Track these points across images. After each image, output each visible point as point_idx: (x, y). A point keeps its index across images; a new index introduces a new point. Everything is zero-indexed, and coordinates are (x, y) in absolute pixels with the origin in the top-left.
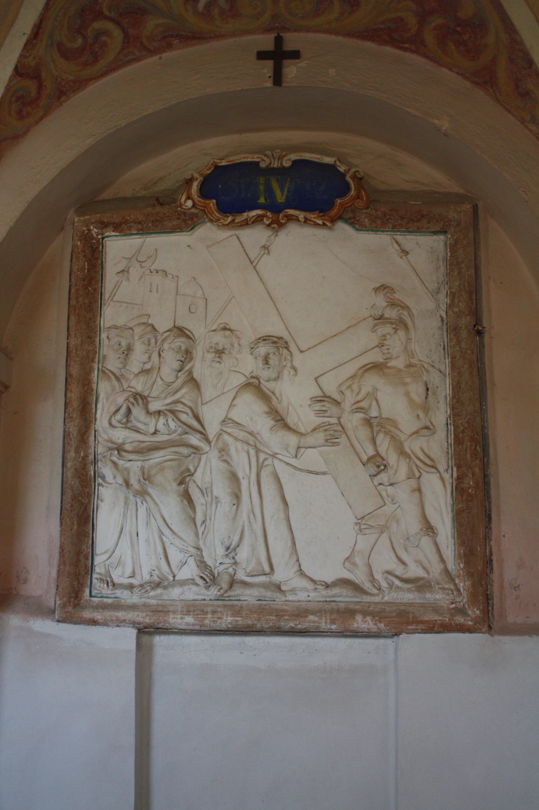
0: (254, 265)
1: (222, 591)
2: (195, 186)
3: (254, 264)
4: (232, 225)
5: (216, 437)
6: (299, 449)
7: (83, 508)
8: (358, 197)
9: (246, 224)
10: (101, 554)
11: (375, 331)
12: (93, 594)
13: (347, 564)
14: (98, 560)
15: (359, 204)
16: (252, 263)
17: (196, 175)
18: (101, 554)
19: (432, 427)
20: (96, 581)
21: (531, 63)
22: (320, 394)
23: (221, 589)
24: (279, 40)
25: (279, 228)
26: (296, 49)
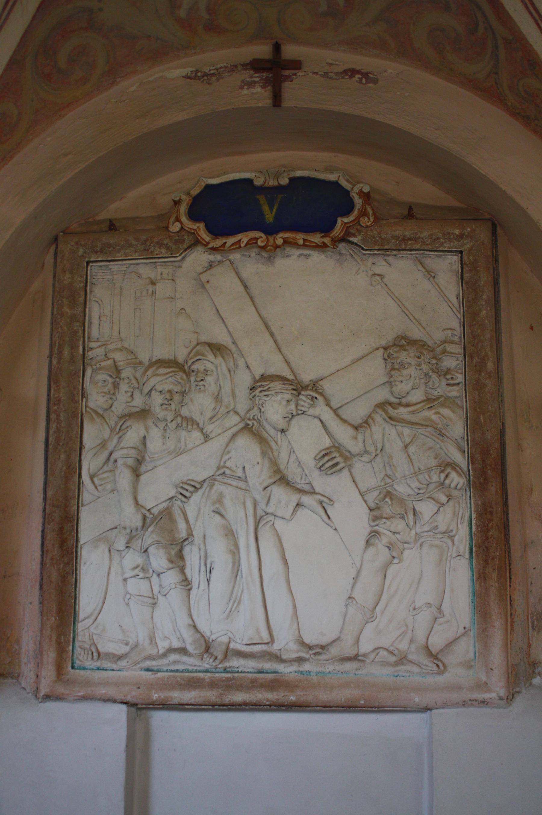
1: (217, 662)
2: (183, 208)
8: (363, 213)
10: (85, 618)
12: (76, 665)
14: (80, 626)
15: (364, 221)
17: (184, 197)
18: (85, 618)
20: (79, 649)
23: (216, 658)
24: (277, 48)
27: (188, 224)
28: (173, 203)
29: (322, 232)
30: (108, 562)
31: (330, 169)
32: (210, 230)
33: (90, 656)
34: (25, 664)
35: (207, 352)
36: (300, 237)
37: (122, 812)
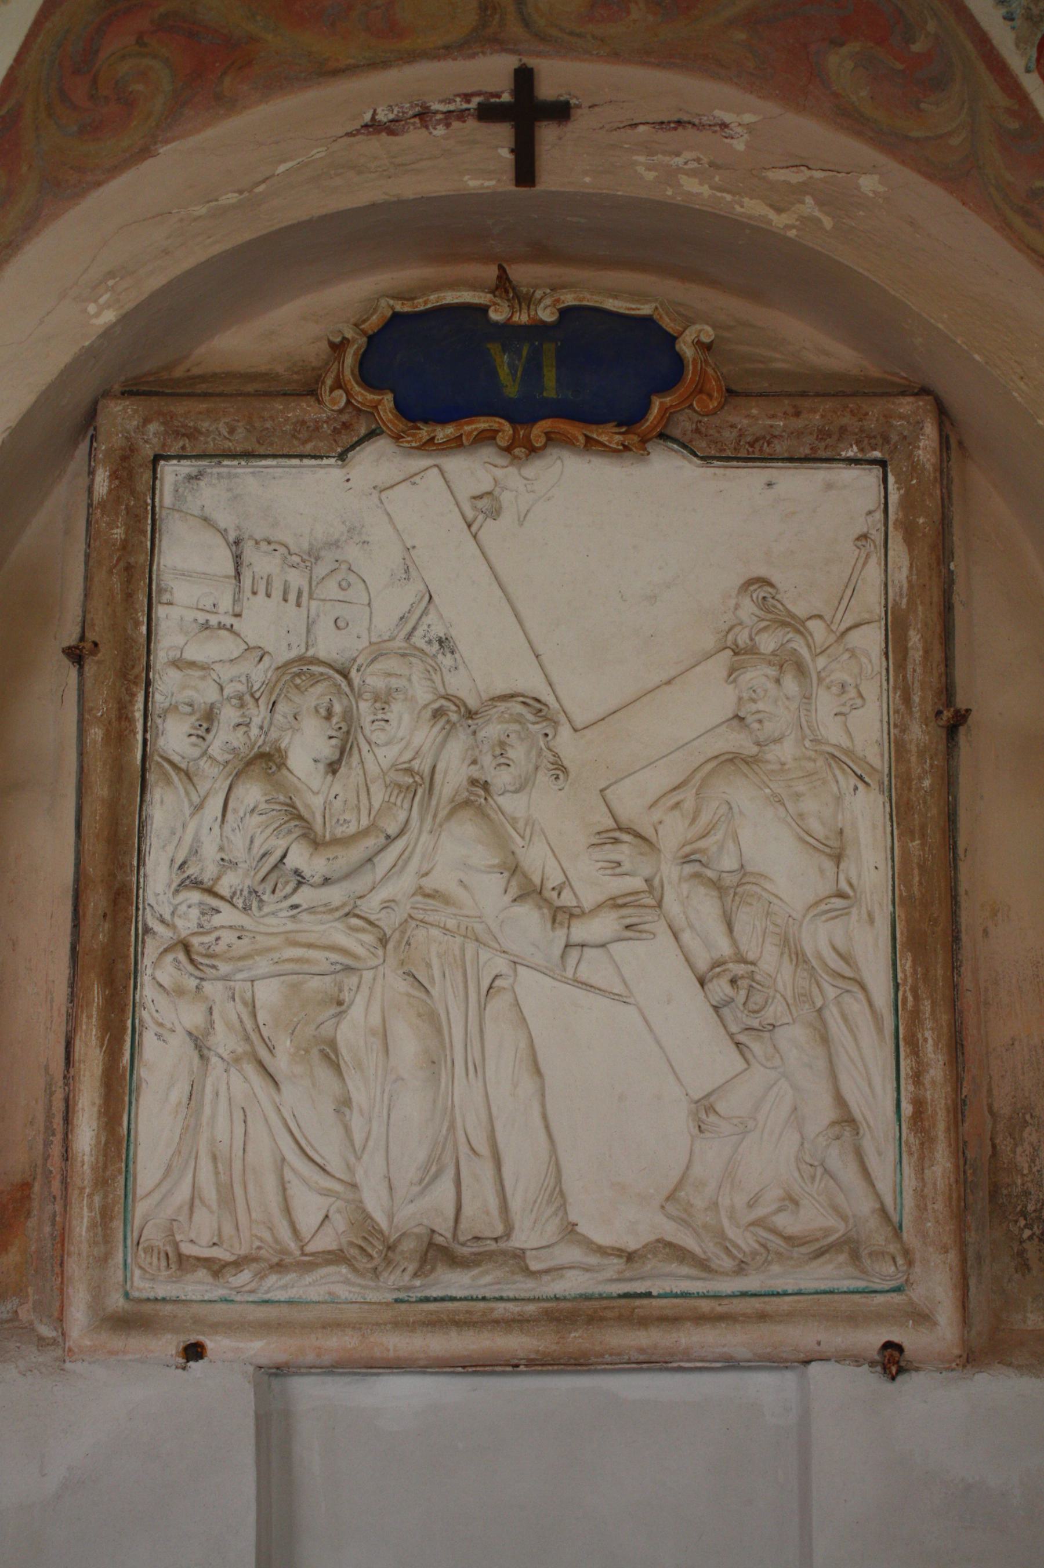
0: (474, 533)
2: (350, 360)
3: (474, 528)
4: (429, 446)
5: (944, 450)
6: (568, 949)
7: (422, 924)
9: (456, 444)
11: (735, 681)
13: (670, 1208)
16: (469, 526)
19: (851, 893)
21: (1037, 117)
22: (611, 824)
24: (524, 78)
25: (527, 456)
26: (537, 180)
27: (363, 396)
28: (328, 349)
29: (620, 425)
30: (886, 1288)
31: (642, 297)
32: (402, 409)
33: (164, 1263)
34: (183, 1288)
35: (935, 1184)
36: (576, 431)
37: (251, 1558)
